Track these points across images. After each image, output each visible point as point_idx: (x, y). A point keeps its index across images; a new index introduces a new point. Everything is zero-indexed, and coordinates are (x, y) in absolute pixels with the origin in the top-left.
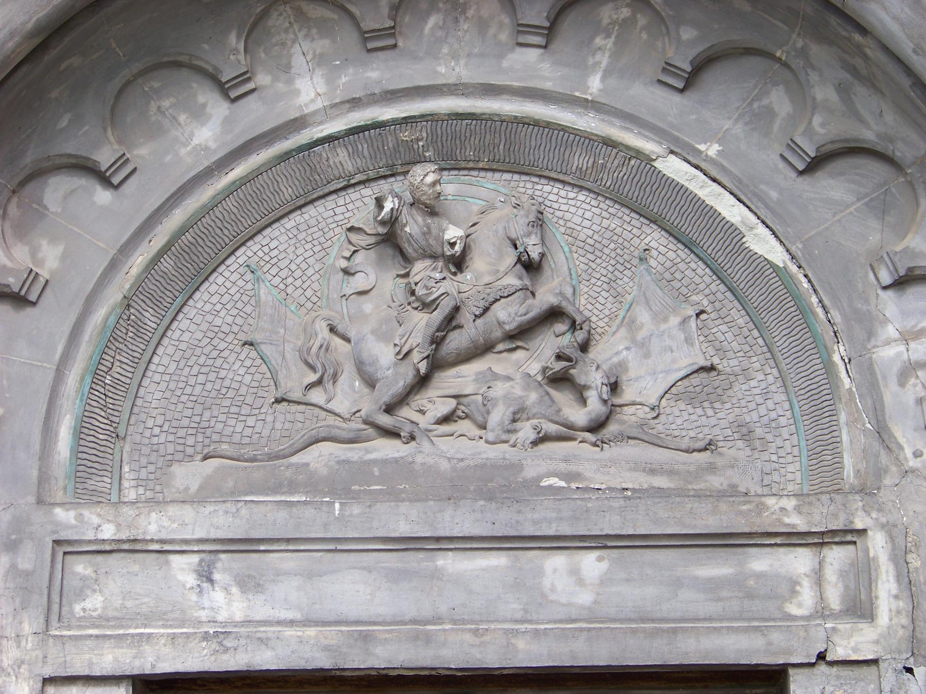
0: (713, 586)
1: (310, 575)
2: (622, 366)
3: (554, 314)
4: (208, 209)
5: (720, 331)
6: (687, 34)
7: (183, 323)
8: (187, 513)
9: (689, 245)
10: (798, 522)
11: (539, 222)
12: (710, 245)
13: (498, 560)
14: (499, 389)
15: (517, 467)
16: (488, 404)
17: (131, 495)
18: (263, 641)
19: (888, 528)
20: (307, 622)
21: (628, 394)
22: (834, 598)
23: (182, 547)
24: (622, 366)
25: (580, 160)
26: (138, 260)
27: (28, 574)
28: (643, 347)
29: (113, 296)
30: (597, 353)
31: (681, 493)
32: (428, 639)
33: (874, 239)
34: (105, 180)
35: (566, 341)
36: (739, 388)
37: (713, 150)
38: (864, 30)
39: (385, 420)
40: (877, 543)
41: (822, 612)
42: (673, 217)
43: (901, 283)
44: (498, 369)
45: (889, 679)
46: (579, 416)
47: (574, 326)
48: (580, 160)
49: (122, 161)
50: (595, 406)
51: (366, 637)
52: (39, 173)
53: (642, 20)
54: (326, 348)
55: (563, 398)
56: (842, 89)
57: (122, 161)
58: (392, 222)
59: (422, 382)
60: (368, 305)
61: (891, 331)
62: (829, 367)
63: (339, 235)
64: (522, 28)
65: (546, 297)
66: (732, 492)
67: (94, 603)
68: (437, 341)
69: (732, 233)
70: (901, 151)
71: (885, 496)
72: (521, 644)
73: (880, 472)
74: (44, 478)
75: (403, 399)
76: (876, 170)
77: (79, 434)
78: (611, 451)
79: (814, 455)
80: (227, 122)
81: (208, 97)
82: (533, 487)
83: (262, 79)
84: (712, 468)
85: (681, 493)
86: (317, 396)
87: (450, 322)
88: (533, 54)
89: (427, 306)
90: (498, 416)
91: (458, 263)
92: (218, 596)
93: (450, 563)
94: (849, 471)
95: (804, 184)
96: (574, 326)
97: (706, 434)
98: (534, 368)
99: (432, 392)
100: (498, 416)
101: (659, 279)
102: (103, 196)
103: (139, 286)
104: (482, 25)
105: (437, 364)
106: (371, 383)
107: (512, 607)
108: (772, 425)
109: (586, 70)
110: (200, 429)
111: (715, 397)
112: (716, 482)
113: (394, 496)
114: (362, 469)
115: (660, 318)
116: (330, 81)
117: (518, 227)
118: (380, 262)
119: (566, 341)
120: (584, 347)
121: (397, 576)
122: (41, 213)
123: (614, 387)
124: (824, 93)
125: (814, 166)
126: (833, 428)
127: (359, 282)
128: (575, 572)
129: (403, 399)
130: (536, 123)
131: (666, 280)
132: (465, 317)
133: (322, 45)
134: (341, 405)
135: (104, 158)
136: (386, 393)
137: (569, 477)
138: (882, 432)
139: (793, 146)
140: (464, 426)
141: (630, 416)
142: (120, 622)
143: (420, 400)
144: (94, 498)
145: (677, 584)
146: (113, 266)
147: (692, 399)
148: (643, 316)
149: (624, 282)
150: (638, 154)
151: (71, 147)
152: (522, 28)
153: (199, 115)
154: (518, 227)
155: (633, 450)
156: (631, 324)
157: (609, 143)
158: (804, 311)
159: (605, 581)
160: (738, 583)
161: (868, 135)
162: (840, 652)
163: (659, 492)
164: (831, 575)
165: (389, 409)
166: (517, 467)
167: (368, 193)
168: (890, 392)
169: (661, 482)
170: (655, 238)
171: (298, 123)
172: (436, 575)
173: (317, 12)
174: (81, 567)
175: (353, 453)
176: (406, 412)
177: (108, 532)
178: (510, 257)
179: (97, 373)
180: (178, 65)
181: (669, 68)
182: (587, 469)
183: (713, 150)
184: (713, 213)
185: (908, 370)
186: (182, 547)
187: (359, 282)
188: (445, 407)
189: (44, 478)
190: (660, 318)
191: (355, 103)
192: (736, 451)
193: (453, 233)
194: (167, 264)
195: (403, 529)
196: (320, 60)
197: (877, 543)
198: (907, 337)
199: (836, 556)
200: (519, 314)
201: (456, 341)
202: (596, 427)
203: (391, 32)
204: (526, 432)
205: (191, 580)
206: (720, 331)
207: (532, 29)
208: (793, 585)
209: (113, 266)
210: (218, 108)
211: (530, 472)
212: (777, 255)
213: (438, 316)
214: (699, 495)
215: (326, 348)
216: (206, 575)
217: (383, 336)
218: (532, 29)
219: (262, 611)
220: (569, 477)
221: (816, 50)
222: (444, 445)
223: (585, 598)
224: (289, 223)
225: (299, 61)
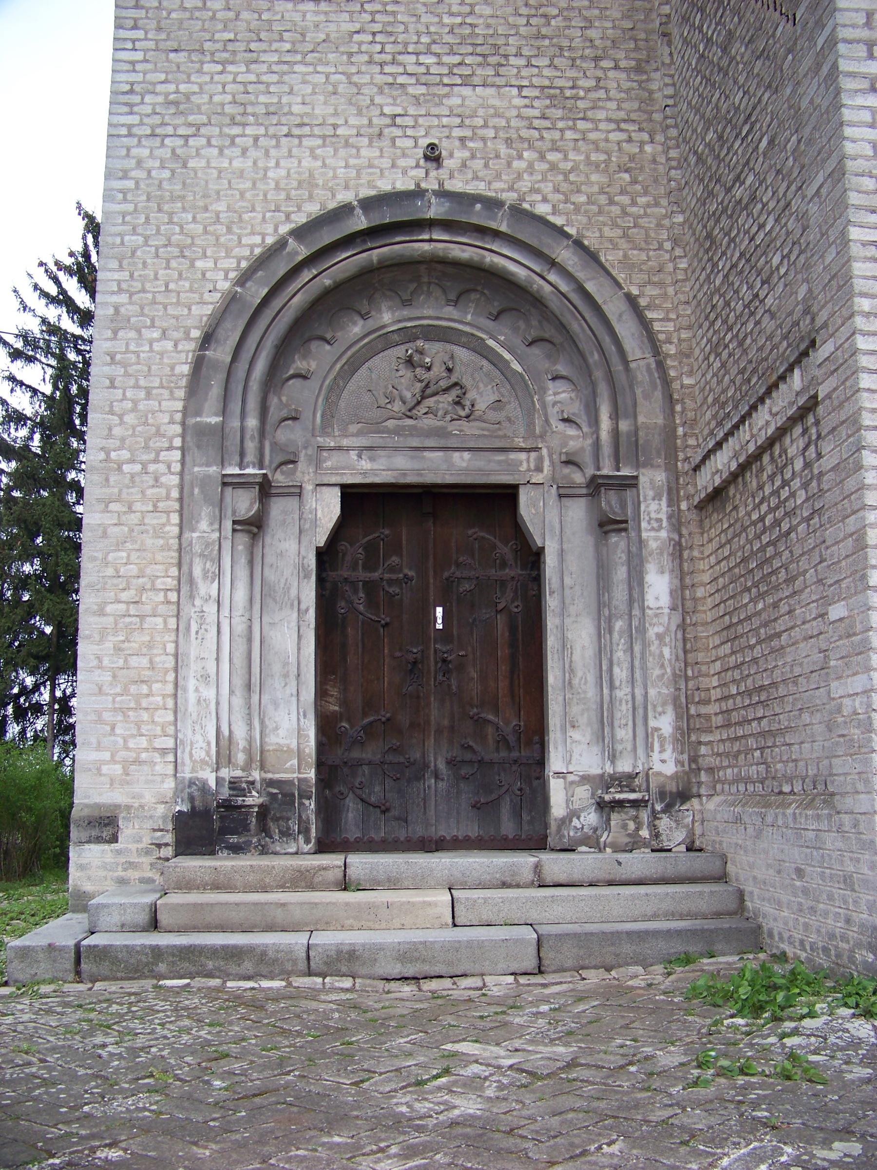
0: (500, 462)
1: (389, 457)
2: (475, 399)
3: (456, 384)
4: (358, 351)
5: (502, 390)
6: (496, 304)
7: (350, 384)
8: (354, 439)
9: (494, 365)
10: (523, 445)
11: (452, 357)
12: (500, 365)
13: (440, 454)
14: (441, 405)
15: (446, 428)
16: (437, 410)
17: (337, 434)
18: (376, 475)
19: (548, 447)
20: (388, 470)
21: (477, 407)
22: (532, 466)
23: (353, 448)
24: (475, 399)
25: (464, 339)
26: (338, 366)
27: (129, 320)
28: (481, 394)
29: (331, 377)
30: (468, 396)
31: (491, 436)
32: (421, 475)
33: (547, 365)
34: (329, 343)
35: (459, 392)
36: (508, 407)
37: (502, 338)
38: (546, 307)
39: (408, 414)
40: (545, 452)
41: (529, 470)
42: (490, 357)
43: (554, 379)
44: (441, 400)
45: (546, 488)
46: (463, 414)
47: (461, 388)
48: (464, 339)
49: (334, 337)
50: (467, 411)
51: (405, 474)
52: (310, 340)
53: (483, 299)
54: (391, 392)
55: (458, 408)
56: (540, 322)
57: (334, 337)
58: (411, 356)
59: (419, 403)
60: (403, 380)
61: (551, 392)
62: (533, 402)
63: (394, 359)
64: (448, 300)
65: (454, 379)
66: (505, 436)
67: (329, 464)
68: (423, 392)
69: (507, 362)
70: (556, 341)
71: (547, 438)
72: (447, 477)
73: (546, 432)
74: (313, 429)
75: (413, 408)
76: (548, 346)
77: (322, 416)
78: (472, 424)
79: (528, 426)
80: (363, 326)
81: (357, 318)
82: (450, 433)
83: (373, 313)
84: (499, 429)
85: (491, 436)
86: (389, 406)
87: (427, 386)
88: (451, 308)
89: (421, 381)
90: (440, 413)
91: (429, 369)
92: (363, 462)
93: (427, 454)
94: (537, 431)
95: (528, 349)
96: (461, 388)
97: (498, 420)
98: (450, 399)
99: (422, 406)
100: (440, 413)
101: (486, 375)
102: (328, 347)
103: (338, 373)
104: (437, 299)
105: (423, 398)
106: (404, 403)
107: (445, 467)
108: (517, 417)
109: (466, 313)
110: (356, 415)
111: (501, 409)
112: (500, 433)
113: (412, 435)
114: (403, 428)
115: (486, 386)
116: (393, 314)
117: (446, 359)
118: (406, 368)
119: (459, 392)
120: (464, 394)
121: (412, 458)
122: (310, 352)
123: (473, 406)
124: (535, 323)
125: (530, 345)
126: (533, 419)
127: (401, 373)
128: (462, 458)
129: (413, 408)
130: (452, 328)
131: (487, 375)
132: (431, 385)
133: (390, 303)
134: (396, 409)
135: (328, 336)
136: (409, 406)
137: (460, 431)
138: (547, 421)
139: (525, 338)
140: (431, 416)
141: (477, 413)
142: (336, 469)
143: (418, 408)
144: (328, 435)
145: (490, 461)
146: (331, 368)
147: (495, 409)
148: (481, 385)
149: (476, 375)
150: (481, 338)
151: (319, 333)
152: (448, 300)
153: (355, 323)
154: (446, 359)
155: (477, 424)
156: (477, 387)
157: (472, 335)
158: (527, 386)
159: (469, 460)
160: (506, 461)
161: (547, 336)
162: (533, 481)
163: (485, 436)
164: (532, 460)
165: (410, 410)
166: (446, 428)
167: (403, 348)
168: (550, 409)
169: (486, 433)
170: (485, 363)
171: (384, 327)
172: (424, 458)
173: (389, 293)
174: (325, 454)
175: (400, 423)
176: (414, 411)
177: (332, 444)
178: (444, 368)
179: (327, 399)
180: (348, 308)
181: (490, 314)
182: (465, 429)
183: (502, 338)
184: (502, 356)
185: (555, 404)
186: (353, 448)
187: (401, 373)
188: (426, 410)
189: (313, 429)
190: (486, 386)
191: (400, 321)
192: (506, 424)
193: (428, 360)
194: (346, 367)
195: (414, 445)
196: (390, 308)
197: (545, 452)
198: (555, 394)
199: (533, 455)
200: (579, 433)
201: (428, 391)
202: (467, 417)
203: (410, 300)
204: (448, 418)
205: (356, 458)
206: (502, 390)
207: (452, 301)
208: (521, 462)
209: (331, 368)
210: (361, 322)
211: (450, 429)
212: (519, 369)
213: (424, 384)
214: (496, 437)
215: (391, 392)
216: (360, 456)
217: (408, 389)
218: (452, 301)
219: (376, 467)
220: (460, 431)
221: (533, 310)
222: (425, 421)
223: (464, 465)
224: (380, 355)
225: (384, 308)
